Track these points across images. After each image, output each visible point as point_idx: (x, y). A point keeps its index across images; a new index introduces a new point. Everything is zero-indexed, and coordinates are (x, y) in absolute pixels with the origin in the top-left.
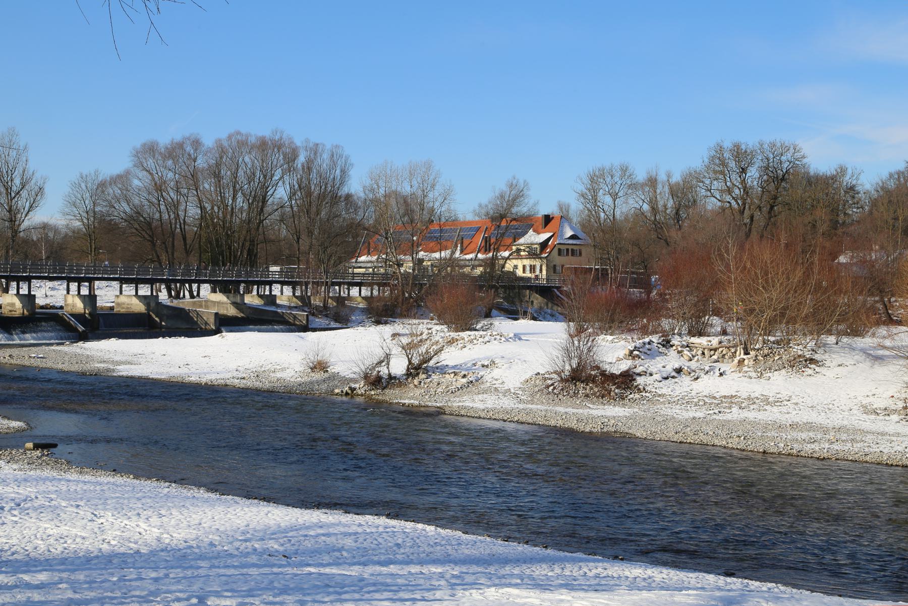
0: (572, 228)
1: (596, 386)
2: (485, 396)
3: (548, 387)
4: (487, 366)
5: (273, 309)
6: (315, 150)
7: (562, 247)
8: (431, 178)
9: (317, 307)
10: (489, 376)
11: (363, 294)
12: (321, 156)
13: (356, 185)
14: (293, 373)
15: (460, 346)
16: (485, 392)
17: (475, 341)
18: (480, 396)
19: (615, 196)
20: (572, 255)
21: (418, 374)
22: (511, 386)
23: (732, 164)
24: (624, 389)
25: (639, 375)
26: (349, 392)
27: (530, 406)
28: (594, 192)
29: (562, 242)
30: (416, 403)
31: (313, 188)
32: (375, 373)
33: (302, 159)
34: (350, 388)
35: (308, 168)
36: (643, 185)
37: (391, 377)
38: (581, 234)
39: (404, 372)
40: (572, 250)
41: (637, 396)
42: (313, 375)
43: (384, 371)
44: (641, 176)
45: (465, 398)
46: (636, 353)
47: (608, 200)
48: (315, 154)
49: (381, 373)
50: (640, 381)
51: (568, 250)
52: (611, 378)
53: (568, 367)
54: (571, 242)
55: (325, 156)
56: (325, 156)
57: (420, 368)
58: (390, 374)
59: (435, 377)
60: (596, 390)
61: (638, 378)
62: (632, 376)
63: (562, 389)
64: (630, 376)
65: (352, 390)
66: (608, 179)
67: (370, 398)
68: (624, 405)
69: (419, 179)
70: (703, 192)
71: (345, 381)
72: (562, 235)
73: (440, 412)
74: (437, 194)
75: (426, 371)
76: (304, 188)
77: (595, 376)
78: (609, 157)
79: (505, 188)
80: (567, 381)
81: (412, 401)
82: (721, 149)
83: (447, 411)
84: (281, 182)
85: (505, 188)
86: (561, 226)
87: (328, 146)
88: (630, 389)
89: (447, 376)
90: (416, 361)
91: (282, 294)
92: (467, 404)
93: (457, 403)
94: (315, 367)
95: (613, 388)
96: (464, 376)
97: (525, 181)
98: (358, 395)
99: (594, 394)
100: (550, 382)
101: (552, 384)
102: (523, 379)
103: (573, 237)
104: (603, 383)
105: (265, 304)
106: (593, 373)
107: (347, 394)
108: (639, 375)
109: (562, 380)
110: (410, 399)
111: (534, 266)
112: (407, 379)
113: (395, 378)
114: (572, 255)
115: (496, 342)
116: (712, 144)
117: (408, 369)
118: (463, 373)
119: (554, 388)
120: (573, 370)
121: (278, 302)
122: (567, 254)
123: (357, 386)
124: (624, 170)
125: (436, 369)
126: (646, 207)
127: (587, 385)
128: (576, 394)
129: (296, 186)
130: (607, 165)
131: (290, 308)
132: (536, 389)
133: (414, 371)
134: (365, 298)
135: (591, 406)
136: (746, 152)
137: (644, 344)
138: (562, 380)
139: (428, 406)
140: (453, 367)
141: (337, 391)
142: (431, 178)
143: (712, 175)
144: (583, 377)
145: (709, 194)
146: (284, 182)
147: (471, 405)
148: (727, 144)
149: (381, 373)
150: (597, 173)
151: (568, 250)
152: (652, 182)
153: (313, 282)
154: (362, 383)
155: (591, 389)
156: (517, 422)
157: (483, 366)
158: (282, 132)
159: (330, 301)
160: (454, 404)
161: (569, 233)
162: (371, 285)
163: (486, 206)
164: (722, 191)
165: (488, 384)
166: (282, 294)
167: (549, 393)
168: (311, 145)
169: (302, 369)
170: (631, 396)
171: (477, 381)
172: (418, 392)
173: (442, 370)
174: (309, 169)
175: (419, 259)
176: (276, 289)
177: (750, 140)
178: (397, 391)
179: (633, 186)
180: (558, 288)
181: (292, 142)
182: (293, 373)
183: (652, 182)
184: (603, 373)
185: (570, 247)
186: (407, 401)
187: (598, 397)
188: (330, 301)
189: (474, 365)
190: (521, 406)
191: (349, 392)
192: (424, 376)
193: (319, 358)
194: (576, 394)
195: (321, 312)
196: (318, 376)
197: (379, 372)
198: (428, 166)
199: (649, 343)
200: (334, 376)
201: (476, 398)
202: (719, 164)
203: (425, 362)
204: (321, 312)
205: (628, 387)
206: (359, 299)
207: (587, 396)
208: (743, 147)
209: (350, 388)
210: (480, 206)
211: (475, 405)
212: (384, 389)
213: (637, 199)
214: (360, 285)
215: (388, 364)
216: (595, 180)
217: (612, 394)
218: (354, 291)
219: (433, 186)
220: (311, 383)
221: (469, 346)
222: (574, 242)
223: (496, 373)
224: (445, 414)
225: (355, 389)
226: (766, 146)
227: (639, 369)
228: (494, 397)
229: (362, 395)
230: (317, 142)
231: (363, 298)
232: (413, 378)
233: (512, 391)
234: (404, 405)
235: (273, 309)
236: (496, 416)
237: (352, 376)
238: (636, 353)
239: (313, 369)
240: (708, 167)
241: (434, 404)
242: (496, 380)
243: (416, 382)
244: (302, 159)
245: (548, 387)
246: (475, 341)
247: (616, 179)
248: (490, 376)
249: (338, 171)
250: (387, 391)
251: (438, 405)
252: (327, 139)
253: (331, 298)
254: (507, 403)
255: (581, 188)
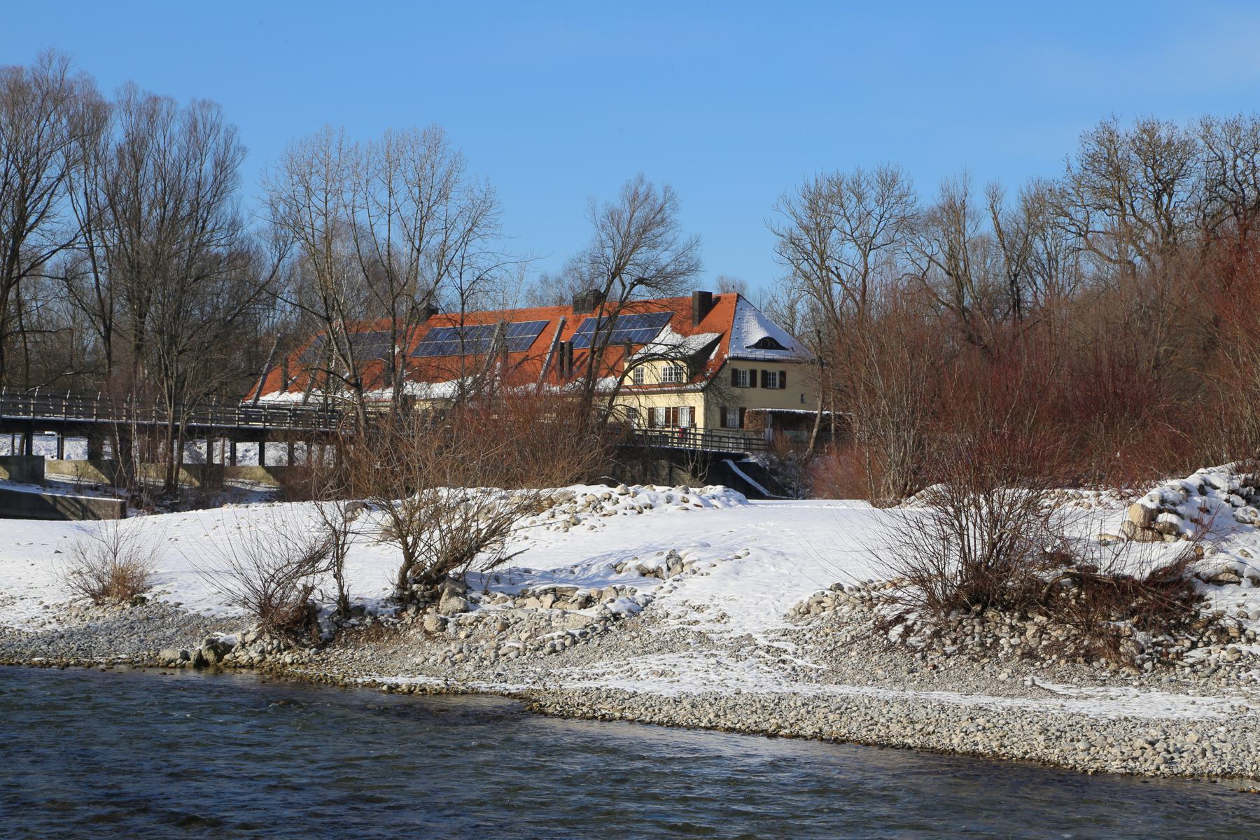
0: (763, 323)
1: (1060, 622)
2: (670, 658)
3: (884, 626)
4: (656, 573)
5: (33, 489)
6: (151, 111)
7: (741, 366)
8: (441, 171)
9: (152, 490)
10: (670, 599)
11: (270, 462)
12: (165, 128)
13: (252, 209)
14: (36, 610)
15: (561, 518)
16: (666, 645)
17: (608, 506)
18: (654, 660)
19: (867, 245)
20: (765, 385)
21: (436, 597)
22: (751, 627)
23: (1138, 175)
24: (1167, 630)
25: (1215, 581)
26: (210, 656)
27: (830, 689)
28: (820, 232)
29: (740, 354)
30: (436, 682)
31: (145, 208)
32: (294, 596)
33: (116, 134)
34: (213, 645)
35: (135, 152)
36: (933, 219)
37: (346, 608)
38: (783, 339)
39: (391, 591)
40: (764, 373)
41: (1219, 654)
42: (98, 612)
43: (325, 588)
44: (927, 198)
45: (600, 667)
46: (1165, 518)
47: (851, 252)
48: (151, 119)
49: (315, 596)
50: (1222, 601)
51: (753, 373)
52: (1118, 590)
53: (954, 566)
54: (760, 354)
55: (176, 128)
56: (176, 128)
57: (442, 579)
58: (343, 599)
59: (493, 607)
60: (1057, 633)
61: (1211, 593)
62: (1191, 588)
63: (937, 634)
64: (1181, 584)
65: (221, 649)
66: (851, 205)
67: (278, 672)
68: (1179, 686)
69: (410, 175)
70: (1071, 240)
71: (195, 624)
72: (739, 339)
73: (526, 708)
74: (453, 211)
75: (463, 586)
76: (118, 208)
77: (1055, 587)
78: (852, 156)
79: (619, 203)
80: (952, 604)
81: (421, 680)
82: (1109, 140)
83: (547, 701)
84: (62, 187)
85: (619, 203)
86: (736, 317)
87: (183, 104)
88: (1187, 628)
89: (531, 603)
90: (427, 559)
91: (60, 456)
92: (613, 683)
93: (573, 680)
94: (106, 591)
95: (1125, 626)
96: (588, 602)
97: (666, 189)
98: (237, 666)
99: (1056, 647)
100: (889, 612)
101: (900, 619)
102: (789, 606)
103: (765, 344)
104: (1084, 609)
105: (12, 479)
106: (1048, 576)
107: (201, 663)
108: (1215, 581)
109: (932, 603)
110: (411, 672)
111: (676, 410)
112: (398, 614)
113: (361, 610)
114: (765, 385)
115: (671, 508)
116: (1092, 127)
117: (403, 583)
118: (583, 592)
119: (908, 631)
120: (973, 568)
121: (49, 475)
122: (753, 384)
123: (236, 637)
124: (889, 182)
125: (491, 582)
126: (938, 275)
127: (1024, 618)
128: (989, 649)
129: (102, 198)
130: (848, 172)
131: (79, 489)
132: (844, 636)
133: (421, 588)
134: (273, 471)
135: (1058, 688)
136: (1170, 143)
137: (1187, 491)
138: (932, 603)
139: (476, 693)
140: (545, 576)
141: (167, 654)
142: (441, 171)
143: (1088, 197)
144: (986, 596)
145: (1081, 243)
146: (71, 190)
147: (629, 686)
148: (1127, 129)
149: (315, 596)
150: (825, 191)
151: (753, 373)
152: (953, 214)
153: (142, 429)
154: (253, 629)
155: (1042, 630)
156: (818, 736)
157: (644, 573)
158: (64, 61)
159: (183, 474)
160: (569, 686)
161: (756, 334)
162: (288, 437)
163: (559, 281)
164: (1118, 236)
165: (674, 624)
166: (60, 456)
167: (891, 647)
168: (141, 98)
169: (65, 599)
170: (1198, 654)
171: (633, 613)
172: (437, 652)
173: (516, 585)
174: (138, 163)
175: (405, 398)
176: (43, 445)
177: (1179, 123)
178: (367, 652)
179: (908, 224)
180: (737, 458)
181: (93, 92)
182: (36, 610)
183: (953, 214)
184: (1086, 578)
185: (759, 367)
186: (403, 681)
187: (1072, 659)
188: (183, 474)
189: (615, 568)
190: (807, 690)
191: (210, 656)
192: (456, 603)
193: (121, 560)
194: (989, 649)
195: (161, 498)
196: (109, 614)
197: (308, 590)
198: (434, 143)
199: (1202, 490)
200: (168, 613)
201: (638, 663)
202: (1108, 169)
203: (458, 561)
204: (161, 498)
205: (1180, 626)
206: (261, 472)
207: (1030, 654)
208: (1163, 134)
209: (213, 645)
210: (545, 280)
211: (643, 688)
212: (322, 645)
213: (916, 255)
214: (260, 437)
215: (339, 562)
216: (822, 205)
217: (1126, 647)
218: (247, 451)
219: (444, 196)
220: (88, 633)
221: (590, 519)
222: (770, 354)
223: (693, 589)
224: (542, 713)
225: (228, 648)
226: (1217, 130)
227: (1214, 563)
228: (700, 662)
229: (251, 666)
230: (159, 92)
231: (269, 469)
232: (421, 610)
233: (762, 642)
234: (392, 689)
235: (33, 489)
236: (730, 720)
237: (222, 612)
238: (1165, 518)
239: (98, 597)
240: (1078, 181)
241: (499, 687)
242: (698, 609)
243: (430, 621)
244: (116, 134)
245: (884, 626)
246: (608, 506)
247: (871, 204)
248: (676, 598)
249: (208, 165)
250: (334, 653)
251: (513, 688)
252: (180, 89)
253: (187, 467)
254: (750, 680)
255: (788, 224)
